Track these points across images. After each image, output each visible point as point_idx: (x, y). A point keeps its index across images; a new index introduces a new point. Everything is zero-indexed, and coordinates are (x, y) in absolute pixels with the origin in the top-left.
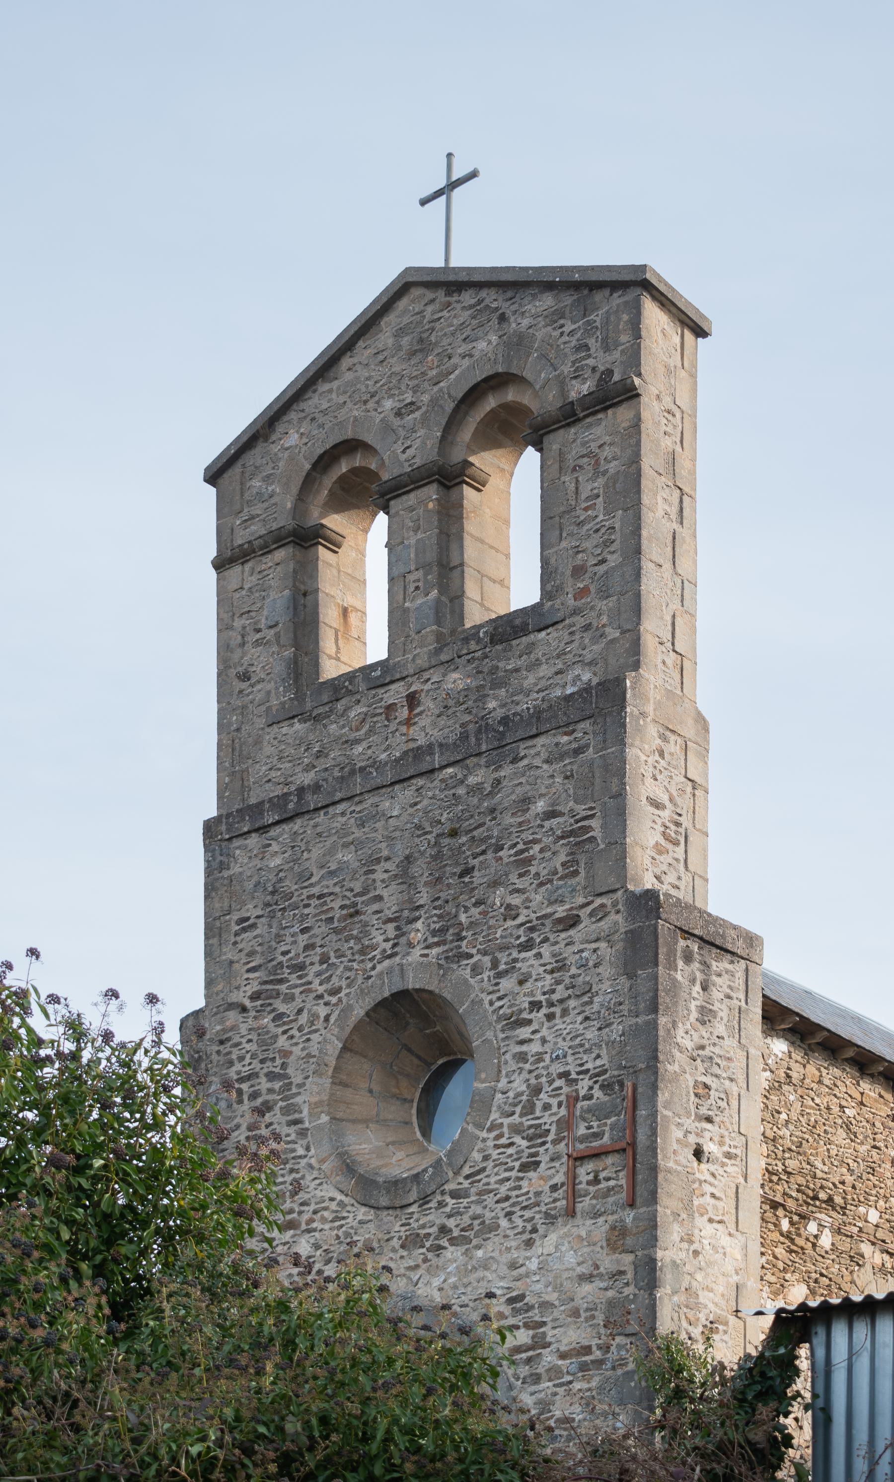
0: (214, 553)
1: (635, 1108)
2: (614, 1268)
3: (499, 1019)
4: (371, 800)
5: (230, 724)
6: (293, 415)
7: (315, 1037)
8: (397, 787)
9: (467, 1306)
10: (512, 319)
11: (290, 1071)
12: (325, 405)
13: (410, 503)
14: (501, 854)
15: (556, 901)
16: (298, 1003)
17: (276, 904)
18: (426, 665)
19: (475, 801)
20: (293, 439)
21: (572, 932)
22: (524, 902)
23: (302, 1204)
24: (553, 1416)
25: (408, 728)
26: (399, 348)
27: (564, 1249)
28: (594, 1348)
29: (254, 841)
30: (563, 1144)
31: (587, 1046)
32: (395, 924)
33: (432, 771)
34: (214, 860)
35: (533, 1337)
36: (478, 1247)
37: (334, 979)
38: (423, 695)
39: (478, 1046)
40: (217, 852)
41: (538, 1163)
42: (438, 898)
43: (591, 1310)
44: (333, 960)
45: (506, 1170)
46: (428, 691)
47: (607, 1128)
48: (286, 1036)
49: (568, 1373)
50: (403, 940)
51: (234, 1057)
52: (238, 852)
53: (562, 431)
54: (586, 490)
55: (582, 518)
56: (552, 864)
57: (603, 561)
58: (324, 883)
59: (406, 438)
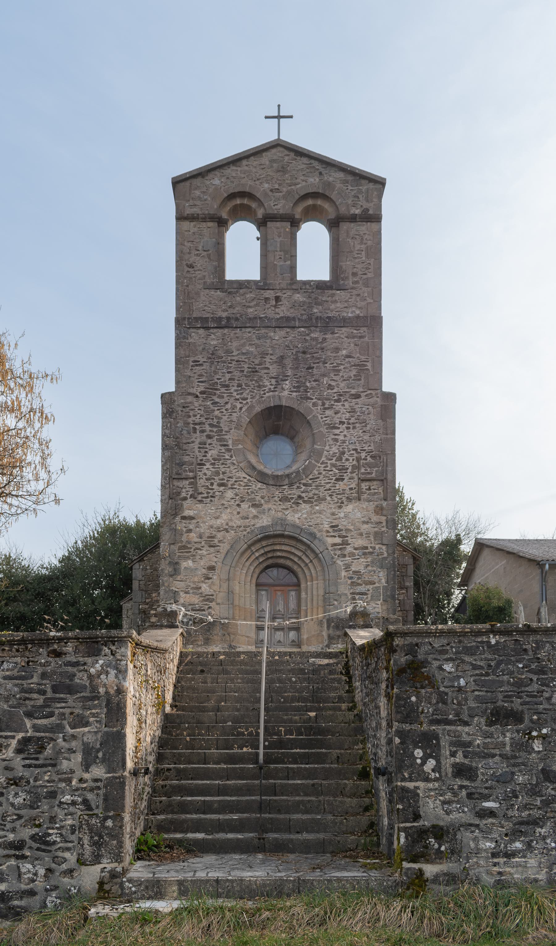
2: (378, 521)
3: (325, 425)
4: (263, 331)
5: (183, 282)
16: (226, 399)
20: (217, 182)
21: (357, 400)
29: (201, 331)
37: (244, 394)
44: (244, 387)
50: (279, 387)
53: (348, 223)
54: (358, 247)
57: (365, 274)
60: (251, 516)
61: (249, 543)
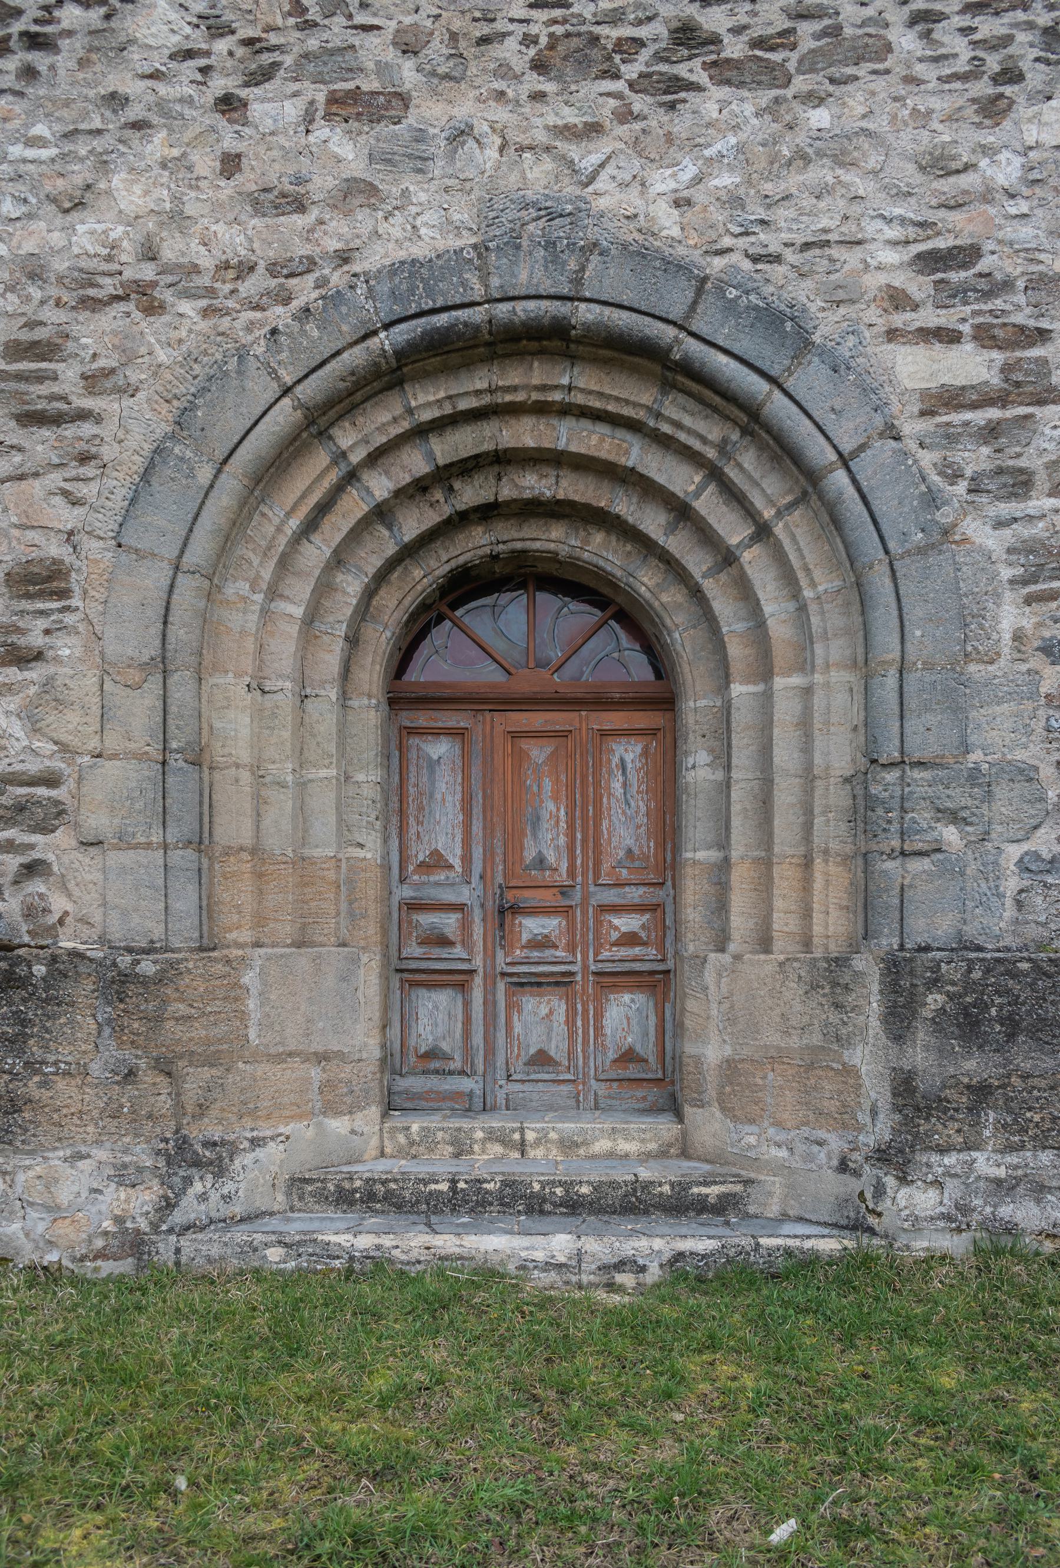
9: (777, 259)
25: (1016, 278)
35: (1006, 369)
60: (322, 184)
61: (310, 390)
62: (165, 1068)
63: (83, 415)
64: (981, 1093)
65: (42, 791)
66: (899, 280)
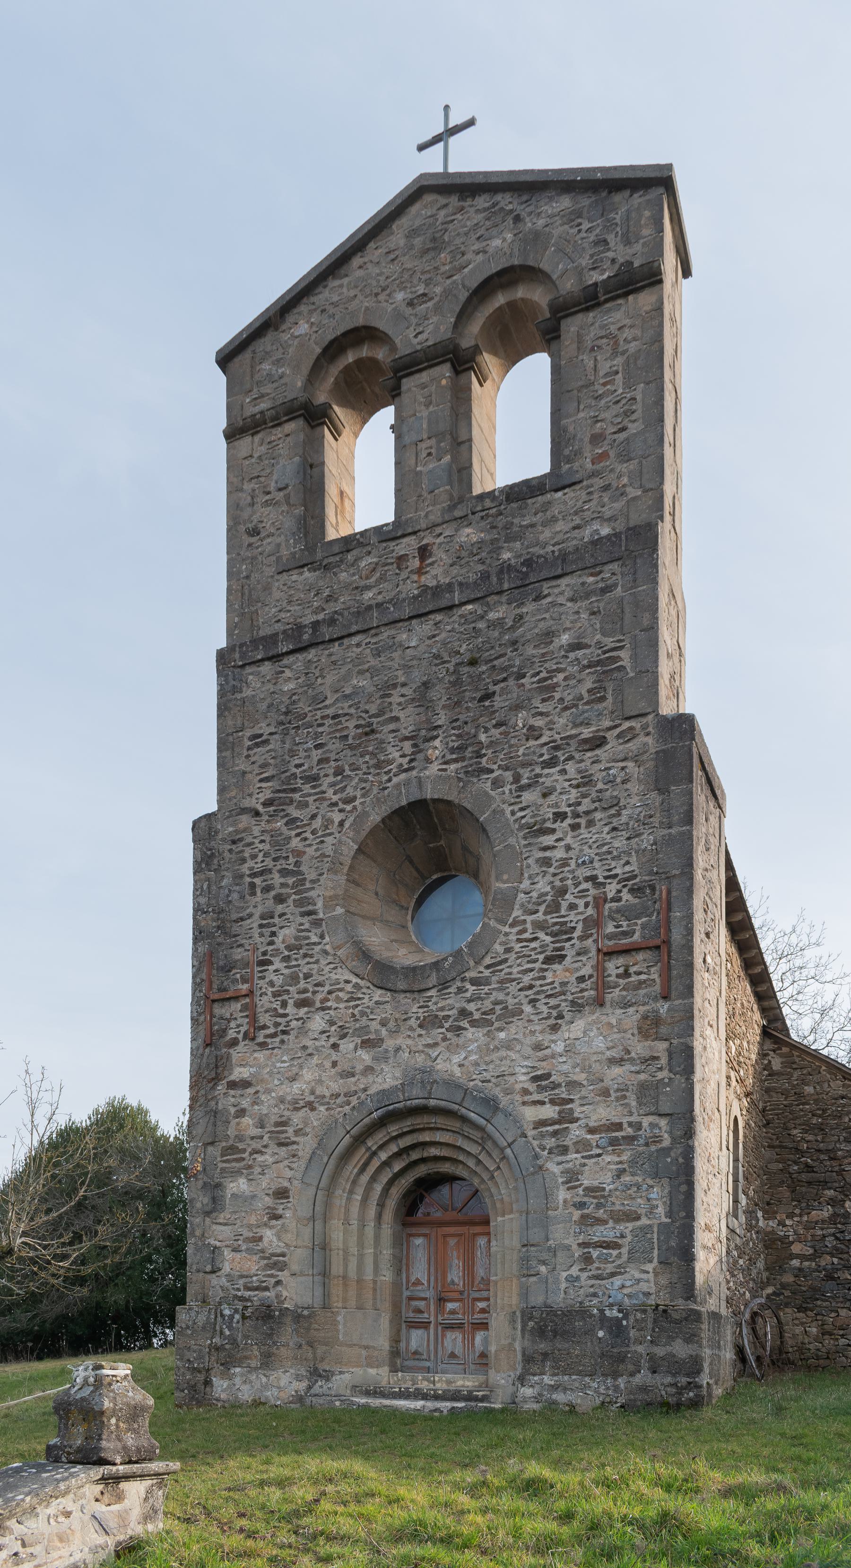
0: (224, 424)
1: (669, 909)
2: (647, 1054)
3: (521, 828)
4: (386, 633)
5: (240, 572)
6: (303, 308)
7: (329, 840)
8: (414, 622)
9: (489, 1081)
10: (527, 219)
11: (303, 868)
12: (335, 298)
13: (423, 380)
14: (523, 681)
15: (581, 724)
16: (312, 809)
17: (289, 723)
18: (440, 520)
19: (496, 634)
20: (303, 328)
21: (598, 752)
22: (547, 724)
23: (316, 985)
24: (581, 1185)
25: (419, 576)
26: (412, 247)
27: (592, 1034)
28: (625, 1126)
29: (267, 668)
30: (590, 940)
31: (615, 853)
32: (411, 742)
33: (450, 608)
34: (227, 683)
35: (560, 1113)
36: (501, 1029)
37: (349, 790)
38: (435, 547)
39: (501, 850)
40: (230, 678)
41: (563, 957)
42: (457, 720)
43: (623, 1090)
45: (528, 962)
46: (440, 544)
47: (638, 928)
48: (299, 839)
49: (598, 1146)
50: (420, 756)
51: (247, 855)
52: (251, 677)
53: (580, 316)
55: (600, 392)
56: (577, 691)
57: (623, 429)
58: (340, 705)
59: (418, 325)
62: (310, 1344)
63: (294, 1143)
64: (545, 1355)
65: (281, 1258)
66: (526, 1085)
